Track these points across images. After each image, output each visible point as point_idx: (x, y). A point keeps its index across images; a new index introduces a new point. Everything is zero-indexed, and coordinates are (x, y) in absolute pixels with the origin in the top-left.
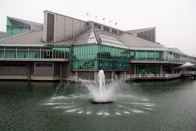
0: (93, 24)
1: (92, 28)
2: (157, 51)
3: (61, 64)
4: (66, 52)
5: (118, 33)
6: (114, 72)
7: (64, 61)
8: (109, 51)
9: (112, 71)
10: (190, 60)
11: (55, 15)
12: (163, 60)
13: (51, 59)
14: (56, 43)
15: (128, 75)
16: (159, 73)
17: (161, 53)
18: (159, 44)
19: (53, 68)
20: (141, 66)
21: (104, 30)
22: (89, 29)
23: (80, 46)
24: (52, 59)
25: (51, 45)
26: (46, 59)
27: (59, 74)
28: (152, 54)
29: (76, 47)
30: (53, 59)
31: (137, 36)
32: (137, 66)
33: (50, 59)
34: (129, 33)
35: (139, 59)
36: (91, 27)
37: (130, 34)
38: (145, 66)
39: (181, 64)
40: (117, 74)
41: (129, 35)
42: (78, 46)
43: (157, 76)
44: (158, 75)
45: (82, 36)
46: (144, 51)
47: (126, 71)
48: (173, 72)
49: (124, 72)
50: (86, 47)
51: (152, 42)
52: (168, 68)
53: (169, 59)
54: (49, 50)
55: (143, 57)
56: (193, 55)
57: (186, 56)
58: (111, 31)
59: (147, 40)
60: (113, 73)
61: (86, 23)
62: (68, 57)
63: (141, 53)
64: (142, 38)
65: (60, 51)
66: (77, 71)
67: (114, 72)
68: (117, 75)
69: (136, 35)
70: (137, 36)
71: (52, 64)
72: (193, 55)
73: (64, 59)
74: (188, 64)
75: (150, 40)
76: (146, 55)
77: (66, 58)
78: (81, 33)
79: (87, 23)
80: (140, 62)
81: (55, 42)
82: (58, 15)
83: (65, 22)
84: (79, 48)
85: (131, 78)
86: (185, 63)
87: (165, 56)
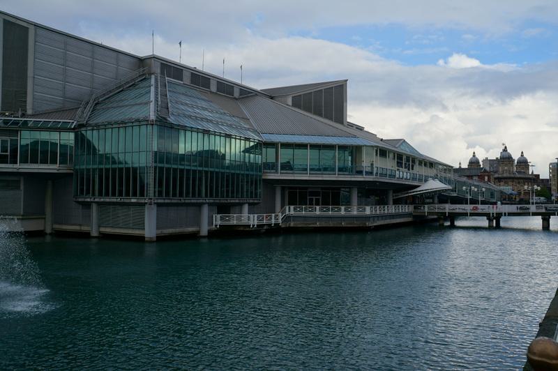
0: (159, 63)
1: (153, 76)
2: (343, 148)
3: (50, 182)
4: (64, 147)
5: (236, 94)
6: (210, 204)
7: (56, 171)
8: (223, 151)
9: (204, 203)
10: (443, 175)
11: (32, 29)
12: (360, 172)
13: (15, 166)
14: (32, 116)
15: (251, 216)
16: (348, 203)
17: (355, 151)
18: (361, 129)
19: (21, 193)
20: (296, 188)
21: (192, 82)
22: (145, 78)
23: (123, 124)
24: (18, 166)
25: (16, 123)
26: (25, 166)
27: (43, 213)
28: (328, 154)
29: (93, 130)
30: (20, 167)
31: (294, 105)
32: (283, 189)
33: (11, 166)
34: (271, 95)
35: (319, 170)
36: (150, 74)
37: (272, 98)
38: (307, 188)
39: (415, 183)
40: (218, 213)
41: (269, 101)
42: (97, 127)
43: (340, 210)
44: (343, 208)
45: (121, 96)
46: (303, 146)
47: (159, 205)
48: (391, 202)
49: (241, 205)
50: (122, 130)
51: (336, 121)
52: (377, 192)
53: (375, 168)
54: (8, 138)
55: (329, 163)
56: (460, 164)
57: (431, 164)
58: (214, 88)
59: (320, 115)
60: (205, 210)
61: (135, 60)
62: (71, 159)
63: (298, 152)
64: (308, 109)
65: (45, 143)
66: (208, 203)
67: (210, 204)
68: (219, 216)
69: (290, 101)
70: (294, 105)
71: (18, 182)
72: (460, 164)
73: (56, 166)
74: (434, 185)
75: (329, 117)
76: (309, 157)
77: (63, 162)
78: (117, 88)
79: (141, 62)
80: (292, 178)
81: (29, 112)
82: (40, 32)
83: (93, 62)
84: (102, 132)
85: (261, 223)
86: (426, 181)
87: (366, 161)
